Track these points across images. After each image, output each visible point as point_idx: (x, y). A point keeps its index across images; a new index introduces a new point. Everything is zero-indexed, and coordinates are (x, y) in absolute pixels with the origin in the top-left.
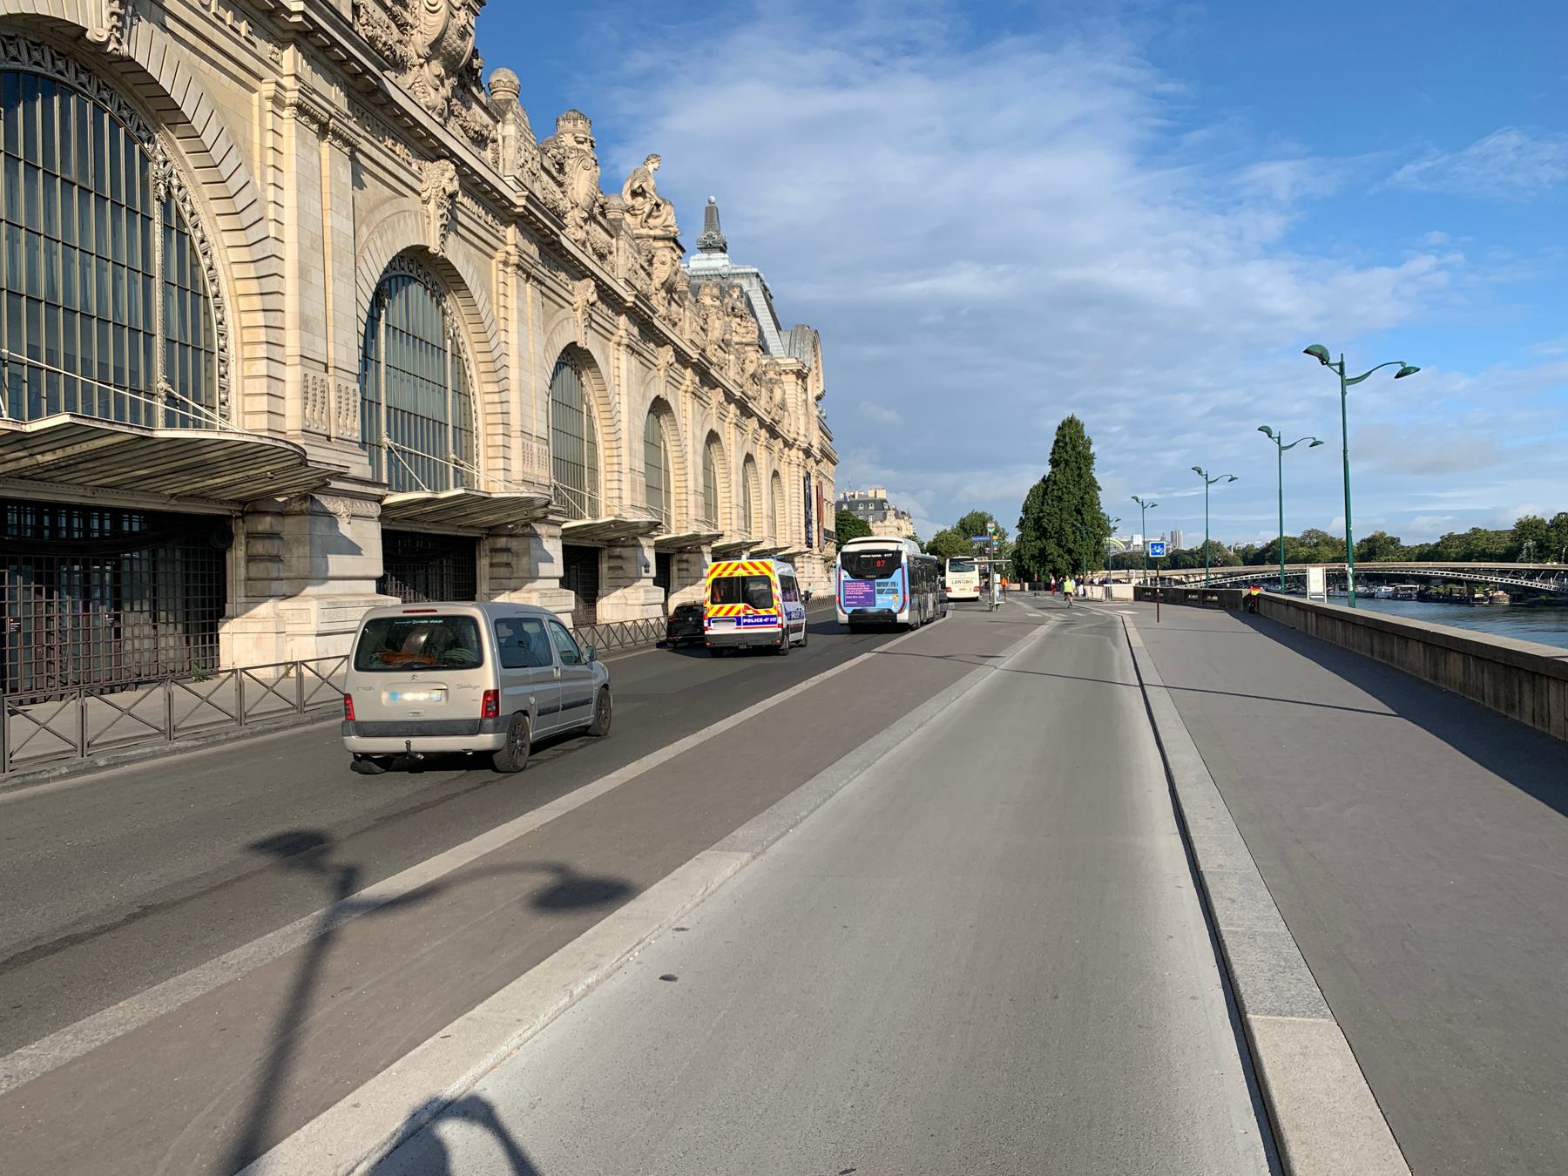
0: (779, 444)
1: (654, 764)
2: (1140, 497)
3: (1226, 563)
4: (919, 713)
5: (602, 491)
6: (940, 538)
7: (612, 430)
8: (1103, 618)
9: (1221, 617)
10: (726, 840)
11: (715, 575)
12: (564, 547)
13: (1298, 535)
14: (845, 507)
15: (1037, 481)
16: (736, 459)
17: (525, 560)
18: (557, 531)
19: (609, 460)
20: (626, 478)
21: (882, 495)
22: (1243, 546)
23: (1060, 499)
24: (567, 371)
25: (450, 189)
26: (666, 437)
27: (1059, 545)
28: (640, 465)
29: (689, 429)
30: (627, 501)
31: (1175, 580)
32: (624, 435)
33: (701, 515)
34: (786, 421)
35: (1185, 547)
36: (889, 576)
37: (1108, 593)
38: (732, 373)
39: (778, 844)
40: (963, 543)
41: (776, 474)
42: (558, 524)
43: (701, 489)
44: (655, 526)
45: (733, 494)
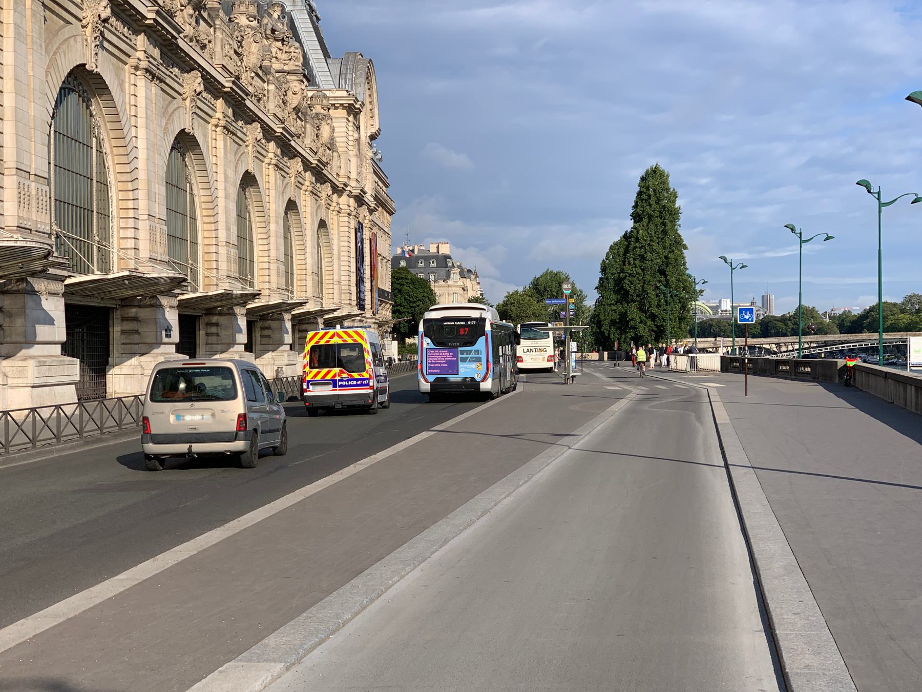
0: (327, 189)
1: (186, 556)
2: (729, 257)
3: (821, 331)
4: (482, 500)
5: (114, 240)
6: (511, 300)
7: (127, 168)
8: (687, 391)
9: (815, 390)
10: (255, 649)
11: (313, 343)
12: (67, 306)
13: (899, 301)
14: (403, 264)
15: (617, 237)
16: (275, 206)
17: (19, 322)
18: (59, 288)
19: (123, 204)
20: (143, 225)
21: (445, 250)
22: (839, 312)
23: (643, 258)
24: (73, 97)
25: (103, 16)
26: (250, 207)
27: (641, 309)
28: (161, 211)
29: (220, 170)
30: (144, 254)
31: (768, 349)
32: (142, 174)
33: (234, 270)
34: (335, 163)
35: (777, 313)
36: (472, 343)
37: (693, 363)
38: (272, 105)
39: (317, 652)
40: (536, 306)
41: (322, 224)
42: (61, 279)
43: (234, 240)
44: (178, 283)
45: (272, 247)
